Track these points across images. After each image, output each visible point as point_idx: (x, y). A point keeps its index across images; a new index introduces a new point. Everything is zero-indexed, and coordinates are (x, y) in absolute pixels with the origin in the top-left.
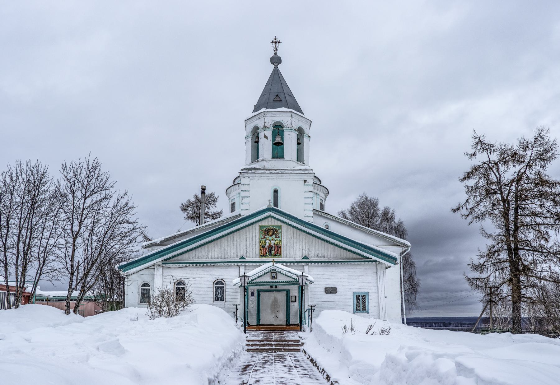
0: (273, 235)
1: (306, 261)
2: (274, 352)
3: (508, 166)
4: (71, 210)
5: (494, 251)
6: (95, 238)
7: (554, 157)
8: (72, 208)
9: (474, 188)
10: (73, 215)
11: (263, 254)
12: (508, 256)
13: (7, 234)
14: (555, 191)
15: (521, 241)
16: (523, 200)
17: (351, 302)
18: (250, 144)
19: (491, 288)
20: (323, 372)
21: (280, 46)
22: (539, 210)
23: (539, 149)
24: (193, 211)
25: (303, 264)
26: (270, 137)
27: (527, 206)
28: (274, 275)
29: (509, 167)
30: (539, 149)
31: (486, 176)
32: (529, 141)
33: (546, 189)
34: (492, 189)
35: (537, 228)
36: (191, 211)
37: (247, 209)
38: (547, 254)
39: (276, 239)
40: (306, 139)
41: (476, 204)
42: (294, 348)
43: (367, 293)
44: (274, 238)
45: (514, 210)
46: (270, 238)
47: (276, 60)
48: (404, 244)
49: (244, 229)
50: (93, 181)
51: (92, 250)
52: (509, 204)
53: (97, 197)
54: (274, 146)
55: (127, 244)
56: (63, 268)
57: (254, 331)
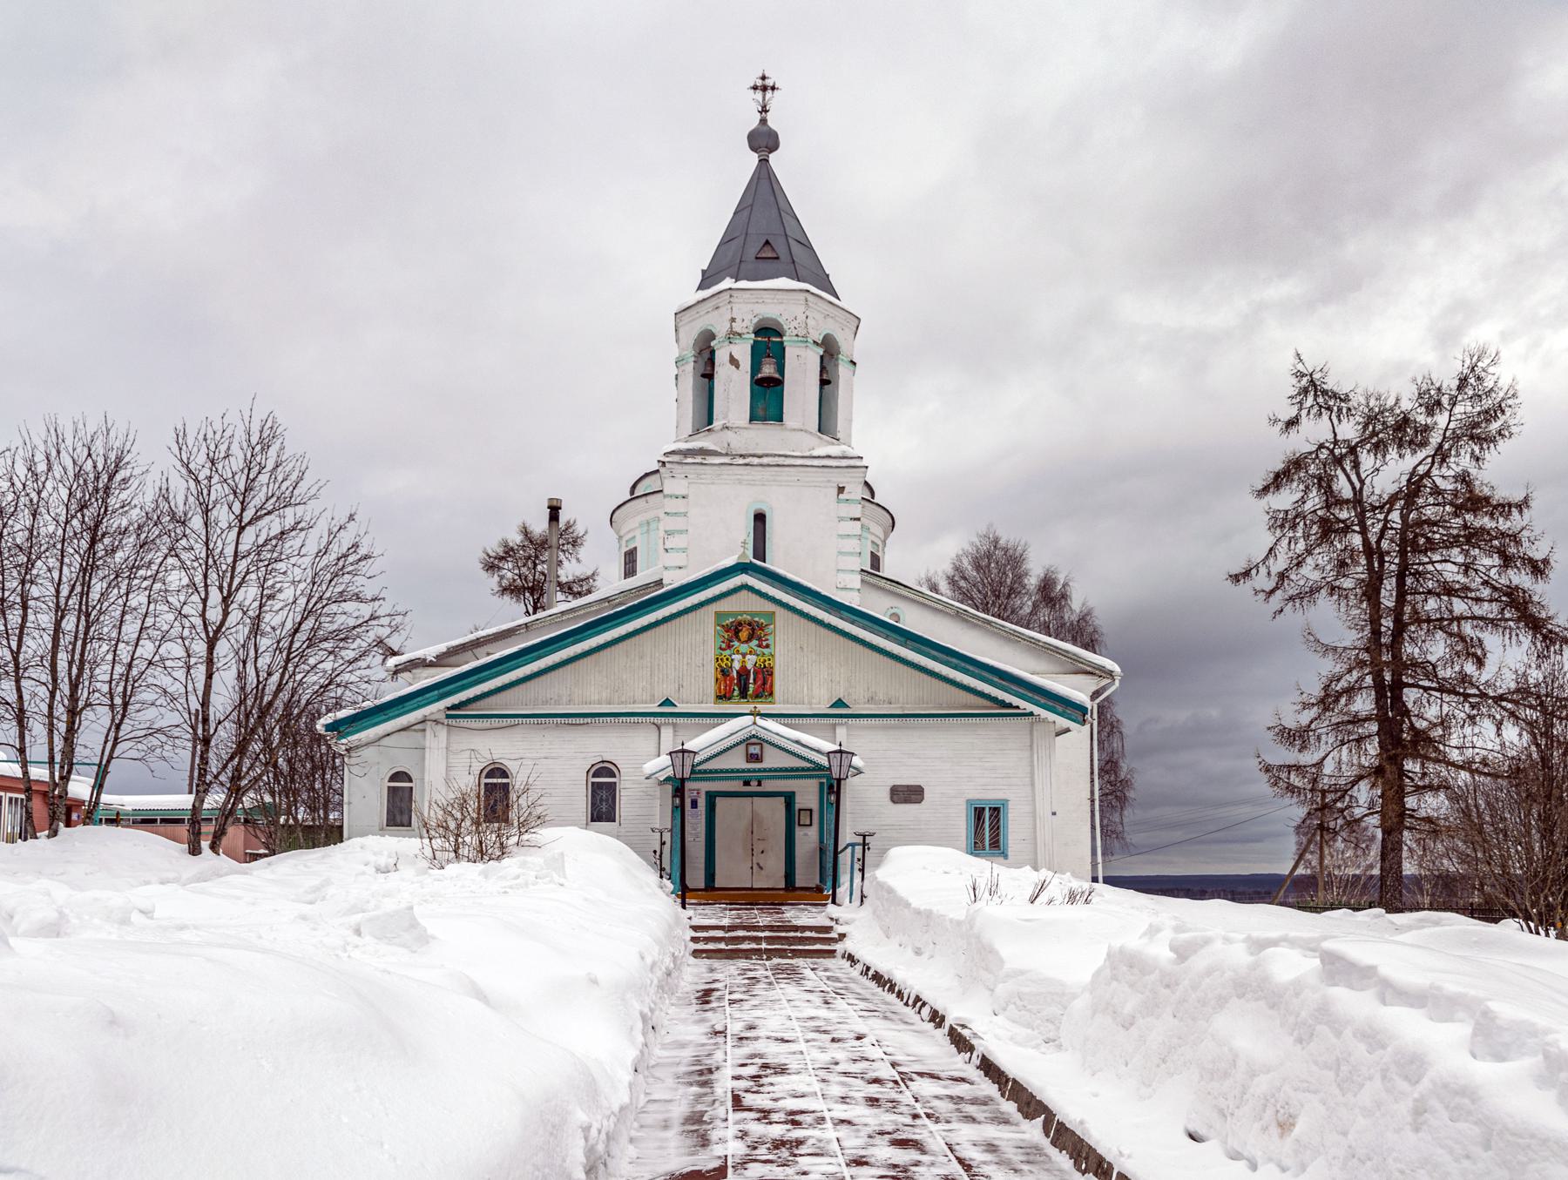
0: (750, 639)
1: (840, 711)
2: (765, 957)
3: (1384, 456)
4: (201, 561)
5: (1337, 691)
6: (264, 643)
7: (1507, 434)
8: (203, 555)
9: (1289, 517)
10: (206, 576)
11: (723, 693)
12: (1373, 706)
13: (22, 627)
14: (1506, 527)
15: (1411, 664)
16: (1420, 552)
17: (961, 824)
18: (689, 381)
19: (1324, 792)
20: (919, 1004)
21: (774, 99)
22: (1461, 578)
23: (1469, 409)
24: (517, 571)
25: (832, 721)
26: (746, 363)
27: (1430, 567)
28: (754, 750)
29: (1388, 457)
30: (1469, 409)
31: (1324, 483)
32: (1444, 386)
33: (1485, 522)
34: (1339, 521)
35: (1456, 629)
36: (509, 572)
37: (681, 565)
38: (1478, 700)
39: (759, 650)
40: (843, 370)
41: (1295, 562)
42: (818, 947)
43: (1005, 802)
44: (756, 648)
45: (1394, 579)
46: (744, 648)
47: (764, 141)
48: (1102, 669)
49: (673, 622)
50: (263, 478)
51: (258, 676)
52: (1382, 563)
53: (272, 525)
54: (756, 387)
55: (356, 660)
56: (177, 726)
57: (701, 904)
